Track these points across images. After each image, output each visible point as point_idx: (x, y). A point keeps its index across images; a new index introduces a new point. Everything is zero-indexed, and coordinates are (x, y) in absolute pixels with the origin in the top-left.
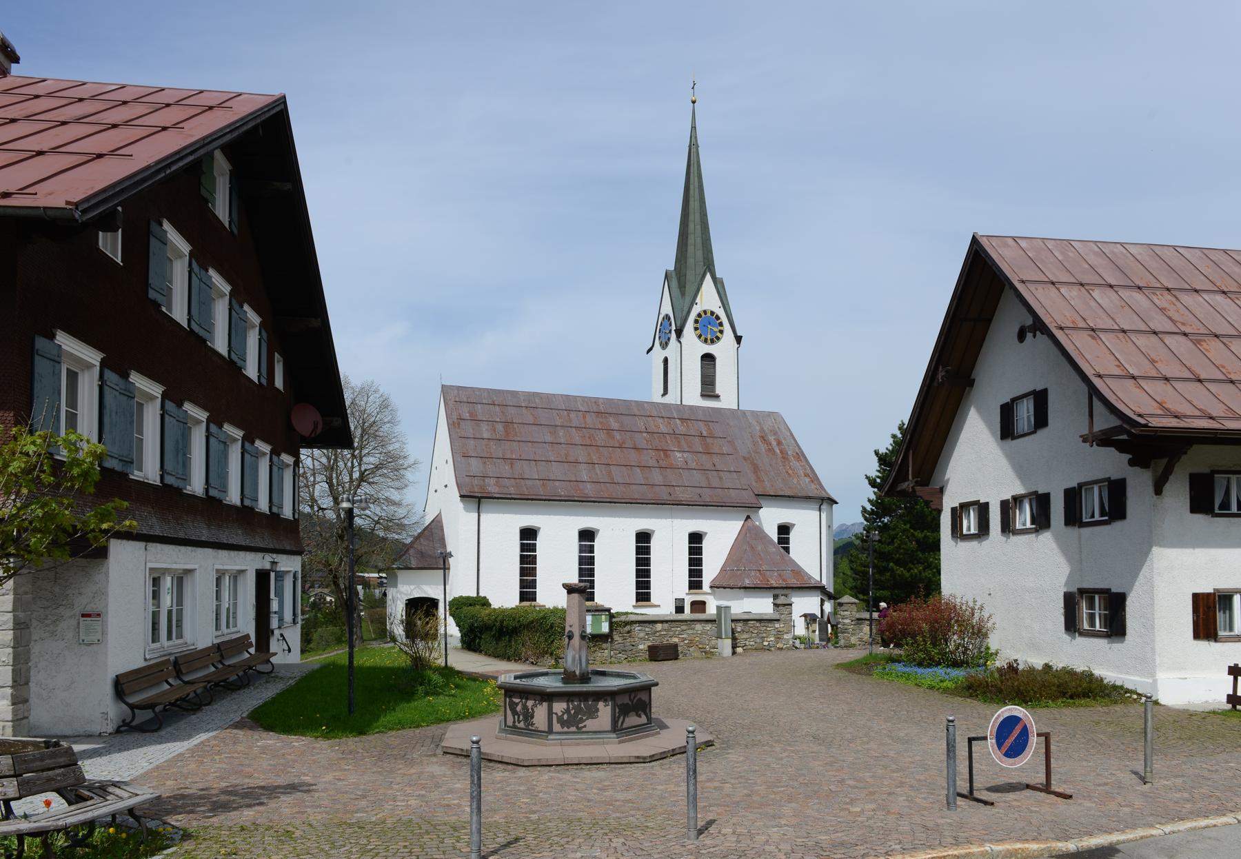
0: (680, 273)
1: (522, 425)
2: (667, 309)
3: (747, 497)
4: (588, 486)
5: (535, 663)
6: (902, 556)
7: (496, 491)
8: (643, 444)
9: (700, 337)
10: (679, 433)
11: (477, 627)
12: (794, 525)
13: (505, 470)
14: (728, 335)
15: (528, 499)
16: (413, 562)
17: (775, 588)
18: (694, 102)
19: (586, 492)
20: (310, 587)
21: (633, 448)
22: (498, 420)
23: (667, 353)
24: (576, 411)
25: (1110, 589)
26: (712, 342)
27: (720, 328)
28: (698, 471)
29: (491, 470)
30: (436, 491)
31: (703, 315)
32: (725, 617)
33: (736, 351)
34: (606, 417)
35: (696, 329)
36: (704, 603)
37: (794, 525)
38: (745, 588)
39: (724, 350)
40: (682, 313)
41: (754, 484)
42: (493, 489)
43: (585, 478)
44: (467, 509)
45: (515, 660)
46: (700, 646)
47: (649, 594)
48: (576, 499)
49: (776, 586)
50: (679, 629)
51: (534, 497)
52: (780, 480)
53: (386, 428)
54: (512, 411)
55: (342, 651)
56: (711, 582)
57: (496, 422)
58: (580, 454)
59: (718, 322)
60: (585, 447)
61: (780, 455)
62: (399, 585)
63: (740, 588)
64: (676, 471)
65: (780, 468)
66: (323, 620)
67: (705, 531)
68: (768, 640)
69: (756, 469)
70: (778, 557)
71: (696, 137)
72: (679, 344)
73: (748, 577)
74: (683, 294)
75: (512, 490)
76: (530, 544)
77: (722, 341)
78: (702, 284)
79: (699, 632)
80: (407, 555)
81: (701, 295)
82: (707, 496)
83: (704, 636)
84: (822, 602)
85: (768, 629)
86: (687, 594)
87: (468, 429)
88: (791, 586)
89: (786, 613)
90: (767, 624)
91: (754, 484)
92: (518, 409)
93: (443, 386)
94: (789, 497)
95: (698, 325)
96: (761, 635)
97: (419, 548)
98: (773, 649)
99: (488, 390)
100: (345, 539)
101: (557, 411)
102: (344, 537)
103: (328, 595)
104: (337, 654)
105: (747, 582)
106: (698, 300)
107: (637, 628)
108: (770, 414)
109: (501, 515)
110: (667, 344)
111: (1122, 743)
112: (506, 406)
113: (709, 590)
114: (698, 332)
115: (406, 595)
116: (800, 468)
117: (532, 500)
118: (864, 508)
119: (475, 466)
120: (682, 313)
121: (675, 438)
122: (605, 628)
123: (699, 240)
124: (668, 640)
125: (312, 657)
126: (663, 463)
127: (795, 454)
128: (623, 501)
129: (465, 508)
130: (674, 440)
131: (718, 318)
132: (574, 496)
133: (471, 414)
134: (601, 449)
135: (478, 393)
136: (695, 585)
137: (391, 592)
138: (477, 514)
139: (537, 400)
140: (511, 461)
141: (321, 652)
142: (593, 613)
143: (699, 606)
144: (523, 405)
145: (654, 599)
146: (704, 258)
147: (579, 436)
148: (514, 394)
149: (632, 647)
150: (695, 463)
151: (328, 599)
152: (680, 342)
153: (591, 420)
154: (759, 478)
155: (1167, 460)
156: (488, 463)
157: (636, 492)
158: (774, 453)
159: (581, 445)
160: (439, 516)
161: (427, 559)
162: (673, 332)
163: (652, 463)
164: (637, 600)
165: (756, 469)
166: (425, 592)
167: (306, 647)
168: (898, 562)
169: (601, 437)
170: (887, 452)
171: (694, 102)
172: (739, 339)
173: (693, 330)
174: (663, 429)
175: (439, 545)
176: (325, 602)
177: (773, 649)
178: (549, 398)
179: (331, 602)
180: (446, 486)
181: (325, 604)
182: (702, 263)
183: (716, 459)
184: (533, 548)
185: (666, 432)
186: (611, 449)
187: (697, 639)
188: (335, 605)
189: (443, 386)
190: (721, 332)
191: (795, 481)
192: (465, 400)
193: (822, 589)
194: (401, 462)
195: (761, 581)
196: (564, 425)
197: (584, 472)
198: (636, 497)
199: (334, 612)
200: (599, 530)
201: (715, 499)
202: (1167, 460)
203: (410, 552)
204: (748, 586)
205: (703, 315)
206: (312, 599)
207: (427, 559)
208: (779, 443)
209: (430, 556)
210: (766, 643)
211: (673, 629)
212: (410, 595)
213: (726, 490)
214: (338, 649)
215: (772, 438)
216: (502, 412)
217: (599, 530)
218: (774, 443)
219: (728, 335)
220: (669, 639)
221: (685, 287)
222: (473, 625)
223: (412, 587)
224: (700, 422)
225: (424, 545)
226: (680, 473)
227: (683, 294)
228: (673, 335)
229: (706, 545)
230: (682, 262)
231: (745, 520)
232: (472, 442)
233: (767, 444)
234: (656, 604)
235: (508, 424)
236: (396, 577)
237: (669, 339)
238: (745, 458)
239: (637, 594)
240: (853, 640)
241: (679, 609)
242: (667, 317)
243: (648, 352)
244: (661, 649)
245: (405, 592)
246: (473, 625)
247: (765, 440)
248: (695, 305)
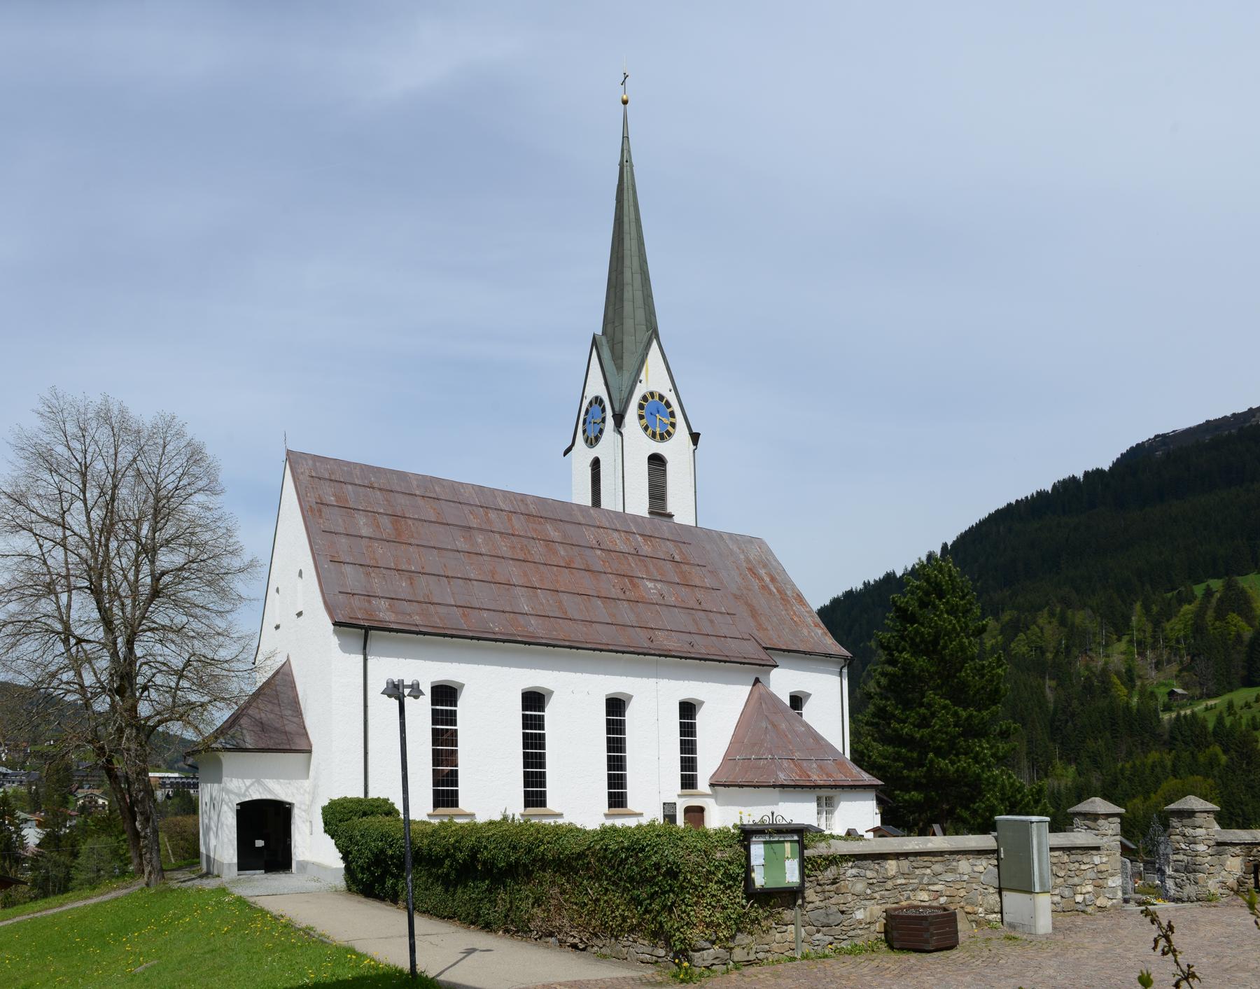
0: (613, 340)
1: (420, 523)
2: (596, 387)
3: (751, 650)
4: (533, 621)
5: (581, 946)
6: (943, 744)
7: (393, 619)
8: (598, 566)
9: (646, 429)
10: (643, 554)
11: (392, 857)
12: (810, 695)
13: (402, 587)
14: (681, 433)
15: (445, 635)
16: (248, 739)
17: (820, 787)
18: (625, 102)
19: (531, 629)
20: (78, 788)
21: (585, 570)
22: (382, 511)
23: (597, 451)
24: (496, 509)
25: (388, 799)
26: (662, 438)
27: (672, 420)
28: (680, 610)
29: (377, 585)
30: (277, 627)
31: (650, 399)
32: (1039, 844)
33: (692, 454)
34: (540, 523)
35: (641, 417)
36: (701, 810)
37: (810, 695)
38: (783, 786)
39: (676, 450)
40: (620, 394)
41: (756, 632)
42: (385, 613)
43: (526, 609)
44: (345, 648)
45: (507, 931)
46: (969, 909)
47: (543, 794)
48: (520, 639)
49: (822, 783)
50: (928, 871)
51: (454, 632)
52: (787, 630)
53: (193, 507)
54: (402, 500)
55: (125, 891)
56: (711, 778)
57: (379, 513)
58: (513, 572)
60: (518, 563)
61: (778, 596)
62: (225, 779)
63: (774, 786)
64: (652, 606)
65: (783, 613)
66: (94, 828)
67: (701, 698)
68: (1084, 891)
69: (754, 613)
70: (812, 740)
71: (629, 151)
72: (619, 436)
73: (783, 770)
74: (619, 368)
75: (417, 619)
77: (674, 438)
78: (647, 354)
79: (966, 877)
80: (237, 727)
82: (702, 646)
83: (975, 886)
85: (1083, 867)
87: (336, 520)
88: (841, 783)
89: (1110, 832)
90: (1079, 858)
91: (756, 632)
92: (410, 497)
93: (289, 453)
94: (805, 653)
95: (644, 412)
96: (1071, 881)
97: (258, 717)
98: (1089, 909)
99: (361, 465)
100: (127, 695)
101: (470, 508)
102: (125, 692)
103: (99, 797)
104: (116, 899)
105: (782, 778)
106: (642, 377)
107: (850, 871)
108: (752, 540)
109: (402, 660)
110: (597, 439)
112: (392, 491)
113: (708, 790)
114: (644, 421)
115: (238, 795)
116: (805, 614)
117: (452, 636)
119: (352, 578)
120: (620, 394)
121: (640, 560)
122: (792, 875)
123: (639, 294)
124: (909, 898)
125: (73, 901)
126: (631, 595)
127: (795, 595)
128: (590, 646)
129: (340, 645)
130: (639, 563)
131: (668, 405)
132: (514, 635)
133: (338, 498)
134: (541, 567)
135: (346, 468)
136: (688, 782)
137: (206, 793)
138: (361, 657)
139: (437, 488)
140: (411, 575)
141: (87, 893)
142: (767, 838)
143: (696, 813)
144: (418, 492)
145: (632, 804)
146: (646, 321)
147: (506, 546)
148: (402, 476)
149: (842, 917)
150: (673, 599)
151: (101, 801)
152: (621, 434)
153: (518, 524)
154: (760, 625)
156: (373, 575)
157: (604, 635)
158: (771, 593)
159: (512, 559)
160: (287, 663)
161: (272, 735)
163: (615, 593)
164: (610, 806)
165: (754, 613)
166: (270, 791)
167: (72, 862)
168: (939, 752)
169: (538, 552)
171: (625, 102)
172: (695, 437)
173: (636, 417)
174: (621, 546)
175: (290, 712)
176: (96, 805)
177: (1089, 909)
178: (454, 486)
179: (103, 806)
180: (300, 614)
181: (96, 808)
182: (644, 327)
183: (699, 594)
184: (451, 718)
185: (627, 551)
186: (555, 568)
187: (962, 893)
188: (109, 810)
189: (289, 453)
190: (673, 425)
191: (805, 632)
192: (327, 476)
194: (225, 561)
195: (800, 776)
196: (483, 527)
197: (522, 599)
198: (604, 641)
199: (109, 819)
200: (552, 692)
201: (713, 651)
203: (242, 721)
204: (786, 783)
205: (650, 399)
206: (81, 802)
207: (272, 735)
208: (773, 579)
209: (276, 729)
210: (1079, 898)
211: (917, 872)
212: (244, 795)
213: (722, 639)
214: (118, 888)
215: (762, 572)
216: (387, 500)
217: (552, 692)
218: (767, 579)
219: (681, 433)
220: (911, 894)
221: (622, 358)
222: (382, 851)
223: (248, 782)
224: (668, 543)
225: (264, 712)
226: (657, 611)
227: (619, 368)
228: (610, 422)
229: (701, 720)
230: (617, 324)
231: (754, 685)
232: (343, 540)
233: (758, 579)
234: (637, 811)
235: (396, 517)
236: (218, 764)
237: (601, 431)
238: (735, 597)
239: (527, 794)
240: (1212, 886)
241: (670, 818)
242: (598, 401)
243: (565, 454)
244: (931, 924)
245: (236, 791)
246: (382, 851)
247: (755, 574)
248: (639, 384)
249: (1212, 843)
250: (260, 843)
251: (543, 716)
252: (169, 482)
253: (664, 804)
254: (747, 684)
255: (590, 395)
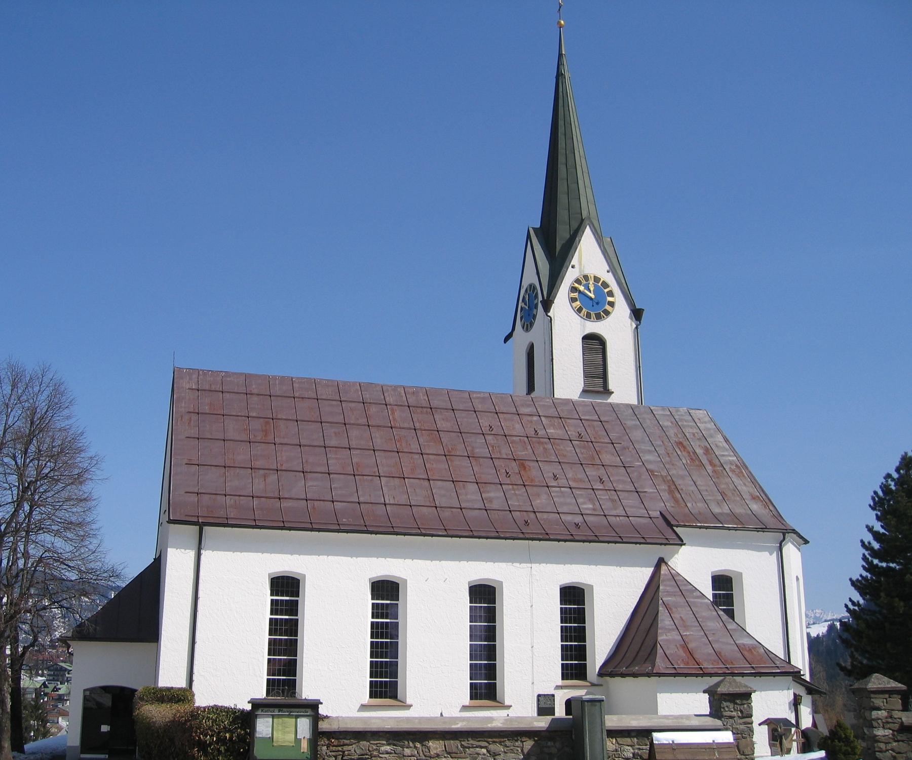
2: (530, 277)
59: (606, 291)
76: (382, 618)
81: (580, 250)
84: (796, 703)
86: (558, 687)
111: (525, 585)
118: (875, 493)
138: (192, 554)
155: (795, 724)
162: (540, 305)
170: (860, 578)
172: (637, 314)
192: (207, 387)
193: (796, 675)
202: (795, 724)
248: (608, 268)
249: (897, 726)
250: (242, 750)
251: (397, 604)
252: (42, 406)
253: (539, 696)
254: (647, 566)
255: (525, 284)
